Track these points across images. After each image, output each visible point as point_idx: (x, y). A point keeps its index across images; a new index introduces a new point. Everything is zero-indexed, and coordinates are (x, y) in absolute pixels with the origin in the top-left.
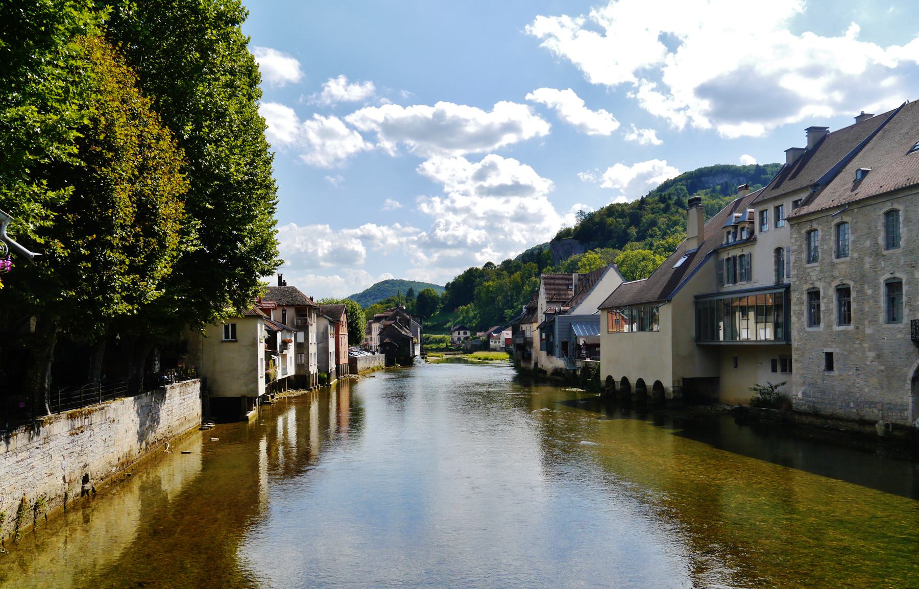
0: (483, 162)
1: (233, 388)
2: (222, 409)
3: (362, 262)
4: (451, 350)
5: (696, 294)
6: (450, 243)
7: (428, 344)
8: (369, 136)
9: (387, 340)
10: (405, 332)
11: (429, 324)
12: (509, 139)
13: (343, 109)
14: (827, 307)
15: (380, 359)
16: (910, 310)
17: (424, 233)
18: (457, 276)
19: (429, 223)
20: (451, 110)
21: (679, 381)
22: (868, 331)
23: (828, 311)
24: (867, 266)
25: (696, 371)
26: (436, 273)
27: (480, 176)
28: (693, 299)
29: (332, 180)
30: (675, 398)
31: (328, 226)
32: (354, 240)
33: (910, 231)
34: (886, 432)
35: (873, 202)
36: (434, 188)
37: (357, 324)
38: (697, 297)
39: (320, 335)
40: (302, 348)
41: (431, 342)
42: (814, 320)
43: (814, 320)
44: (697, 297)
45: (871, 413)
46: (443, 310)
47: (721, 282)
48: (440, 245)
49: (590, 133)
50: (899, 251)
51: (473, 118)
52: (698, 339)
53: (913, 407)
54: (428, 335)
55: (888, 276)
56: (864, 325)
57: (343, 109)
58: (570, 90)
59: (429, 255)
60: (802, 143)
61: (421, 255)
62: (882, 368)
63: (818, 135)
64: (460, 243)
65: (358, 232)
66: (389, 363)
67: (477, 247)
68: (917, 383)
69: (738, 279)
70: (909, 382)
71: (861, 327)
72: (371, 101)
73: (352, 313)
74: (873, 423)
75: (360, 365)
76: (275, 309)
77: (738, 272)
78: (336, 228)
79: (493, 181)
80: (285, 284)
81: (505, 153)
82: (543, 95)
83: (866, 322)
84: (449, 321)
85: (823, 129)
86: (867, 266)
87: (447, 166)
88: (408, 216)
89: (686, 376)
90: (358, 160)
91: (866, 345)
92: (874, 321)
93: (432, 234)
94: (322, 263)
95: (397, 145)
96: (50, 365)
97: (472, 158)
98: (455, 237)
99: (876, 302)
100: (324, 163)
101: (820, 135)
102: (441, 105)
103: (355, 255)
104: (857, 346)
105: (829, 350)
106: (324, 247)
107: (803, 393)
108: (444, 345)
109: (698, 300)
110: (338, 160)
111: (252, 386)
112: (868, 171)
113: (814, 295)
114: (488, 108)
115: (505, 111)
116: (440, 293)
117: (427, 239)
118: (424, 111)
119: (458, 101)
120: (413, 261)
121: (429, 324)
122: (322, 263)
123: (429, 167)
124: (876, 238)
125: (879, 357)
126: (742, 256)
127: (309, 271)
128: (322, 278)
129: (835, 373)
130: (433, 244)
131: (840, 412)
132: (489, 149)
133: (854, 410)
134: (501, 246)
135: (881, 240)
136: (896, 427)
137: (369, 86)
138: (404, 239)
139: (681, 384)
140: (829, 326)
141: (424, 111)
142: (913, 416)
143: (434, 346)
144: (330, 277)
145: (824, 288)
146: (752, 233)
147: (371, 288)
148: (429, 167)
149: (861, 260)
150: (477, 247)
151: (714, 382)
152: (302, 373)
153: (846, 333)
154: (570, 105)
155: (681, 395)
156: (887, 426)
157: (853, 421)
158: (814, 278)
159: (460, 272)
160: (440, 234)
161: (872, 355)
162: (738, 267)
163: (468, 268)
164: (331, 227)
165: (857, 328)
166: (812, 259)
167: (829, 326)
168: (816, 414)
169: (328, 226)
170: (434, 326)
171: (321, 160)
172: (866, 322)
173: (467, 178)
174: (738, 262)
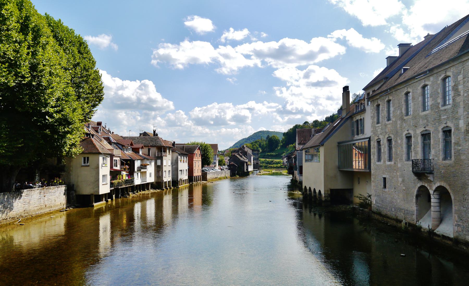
0: (307, 69)
1: (86, 190)
2: (80, 201)
3: (249, 121)
4: (282, 168)
5: (339, 141)
6: (294, 111)
8: (248, 57)
9: (232, 163)
10: (243, 159)
12: (322, 57)
13: (234, 44)
14: (384, 150)
15: (227, 173)
16: (415, 153)
19: (284, 102)
20: (288, 42)
21: (328, 191)
22: (399, 165)
23: (384, 152)
24: (398, 126)
25: (339, 185)
26: (281, 127)
27: (307, 76)
28: (337, 144)
29: (231, 80)
30: (326, 200)
31: (231, 104)
33: (415, 105)
34: (406, 228)
35: (399, 88)
36: (281, 83)
37: (208, 155)
38: (339, 143)
39: (174, 161)
40: (159, 169)
41: (274, 164)
42: (379, 159)
43: (379, 159)
44: (339, 143)
45: (400, 216)
47: (353, 135)
48: (290, 113)
49: (367, 52)
50: (410, 117)
51: (300, 47)
52: (339, 167)
53: (417, 213)
54: (272, 160)
55: (406, 132)
56: (397, 161)
57: (234, 44)
58: (352, 29)
59: (283, 118)
60: (396, 53)
62: (404, 188)
63: (404, 48)
64: (299, 112)
65: (245, 106)
66: (233, 175)
68: (419, 198)
69: (360, 132)
70: (415, 197)
71: (396, 163)
72: (247, 40)
73: (204, 150)
74: (400, 221)
75: (209, 177)
76: (142, 148)
77: (360, 128)
78: (235, 105)
79: (314, 78)
80: (157, 135)
81: (321, 65)
82: (338, 34)
83: (398, 160)
84: (284, 153)
85: (408, 45)
86: (398, 126)
87: (285, 71)
88: (271, 98)
89: (332, 188)
90: (244, 71)
91: (398, 174)
92: (401, 160)
93: (284, 107)
94: (229, 122)
95: (262, 61)
97: (300, 68)
98: (297, 109)
99: (402, 147)
100: (226, 72)
101: (406, 48)
102: (281, 42)
104: (395, 174)
105: (384, 176)
106: (229, 114)
107: (376, 201)
108: (279, 165)
109: (339, 144)
110: (232, 71)
111: (96, 189)
112: (408, 69)
113: (379, 142)
114: (308, 42)
115: (317, 43)
116: (281, 138)
118: (274, 45)
119: (292, 37)
120: (274, 121)
122: (229, 122)
123: (278, 74)
124: (401, 109)
125: (403, 181)
126: (361, 119)
127: (222, 126)
129: (387, 190)
130: (283, 112)
131: (389, 214)
132: (312, 62)
133: (394, 213)
134: (321, 113)
135: (404, 112)
136: (410, 225)
137: (246, 32)
139: (329, 192)
140: (385, 162)
141: (274, 45)
142: (417, 218)
143: (275, 166)
145: (383, 138)
146: (364, 106)
148: (278, 74)
149: (396, 122)
151: (351, 191)
152: (159, 181)
153: (390, 166)
154: (354, 38)
155: (329, 198)
156: (406, 223)
157: (394, 219)
158: (379, 133)
159: (291, 127)
160: (289, 107)
161: (400, 180)
162: (359, 126)
164: (232, 104)
165: (395, 163)
166: (378, 123)
167: (385, 162)
168: (380, 214)
169: (231, 104)
170: (276, 155)
171: (225, 71)
172: (398, 160)
173: (300, 78)
174: (359, 123)
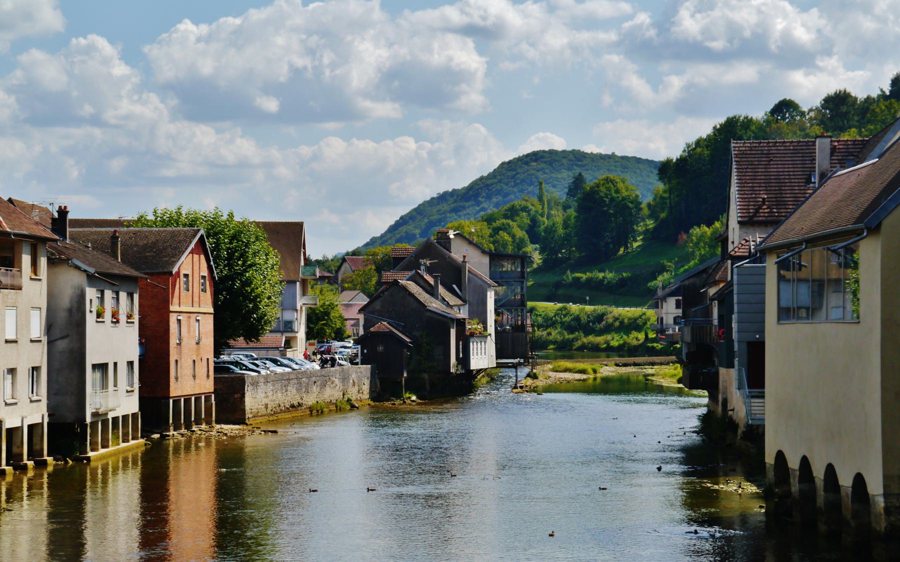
7: (600, 333)
9: (384, 326)
10: (442, 302)
11: (610, 275)
17: (643, 18)
18: (692, 139)
32: (451, 38)
37: (248, 282)
41: (608, 329)
46: (652, 237)
54: (600, 309)
59: (656, 83)
61: (637, 84)
64: (751, 46)
66: (385, 391)
67: (797, 57)
84: (663, 269)
96: (408, 340)
98: (733, 30)
103: (454, 77)
108: (636, 338)
117: (652, 33)
120: (607, 100)
121: (610, 275)
127: (331, 126)
128: (366, 146)
138: (585, 36)
143: (615, 340)
144: (389, 143)
147: (498, 168)
150: (797, 57)
159: (704, 128)
163: (722, 120)
170: (622, 282)
